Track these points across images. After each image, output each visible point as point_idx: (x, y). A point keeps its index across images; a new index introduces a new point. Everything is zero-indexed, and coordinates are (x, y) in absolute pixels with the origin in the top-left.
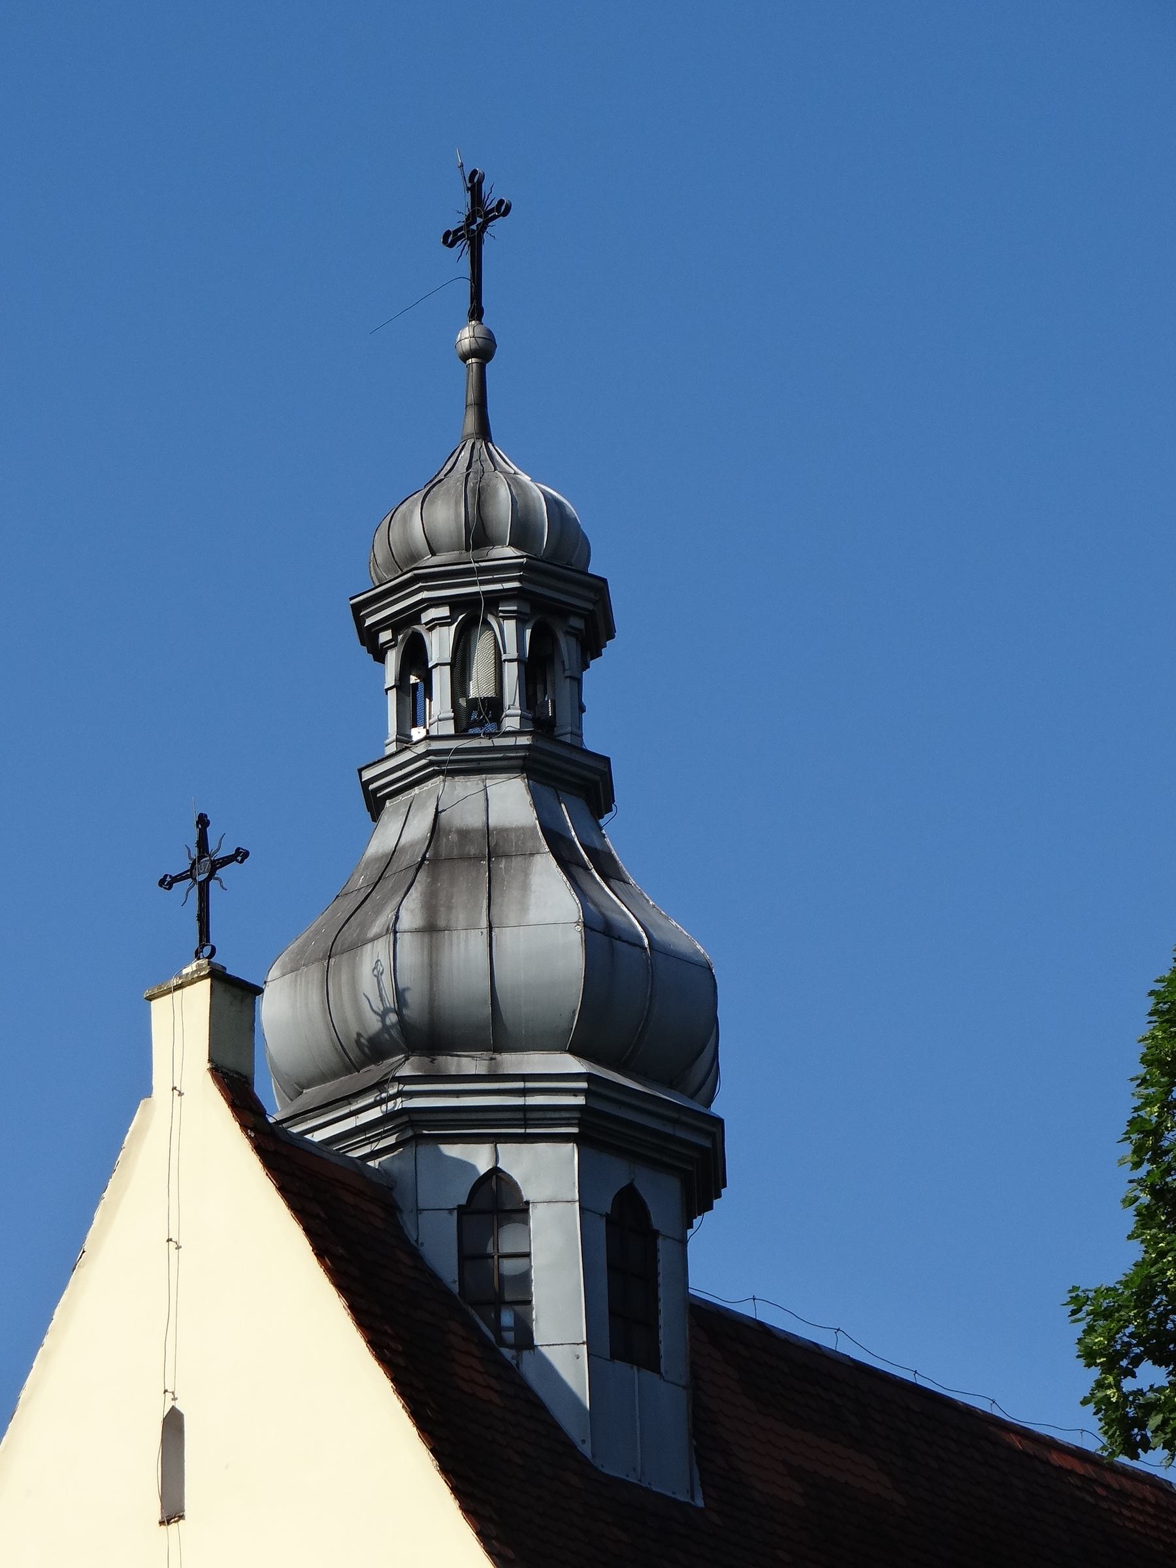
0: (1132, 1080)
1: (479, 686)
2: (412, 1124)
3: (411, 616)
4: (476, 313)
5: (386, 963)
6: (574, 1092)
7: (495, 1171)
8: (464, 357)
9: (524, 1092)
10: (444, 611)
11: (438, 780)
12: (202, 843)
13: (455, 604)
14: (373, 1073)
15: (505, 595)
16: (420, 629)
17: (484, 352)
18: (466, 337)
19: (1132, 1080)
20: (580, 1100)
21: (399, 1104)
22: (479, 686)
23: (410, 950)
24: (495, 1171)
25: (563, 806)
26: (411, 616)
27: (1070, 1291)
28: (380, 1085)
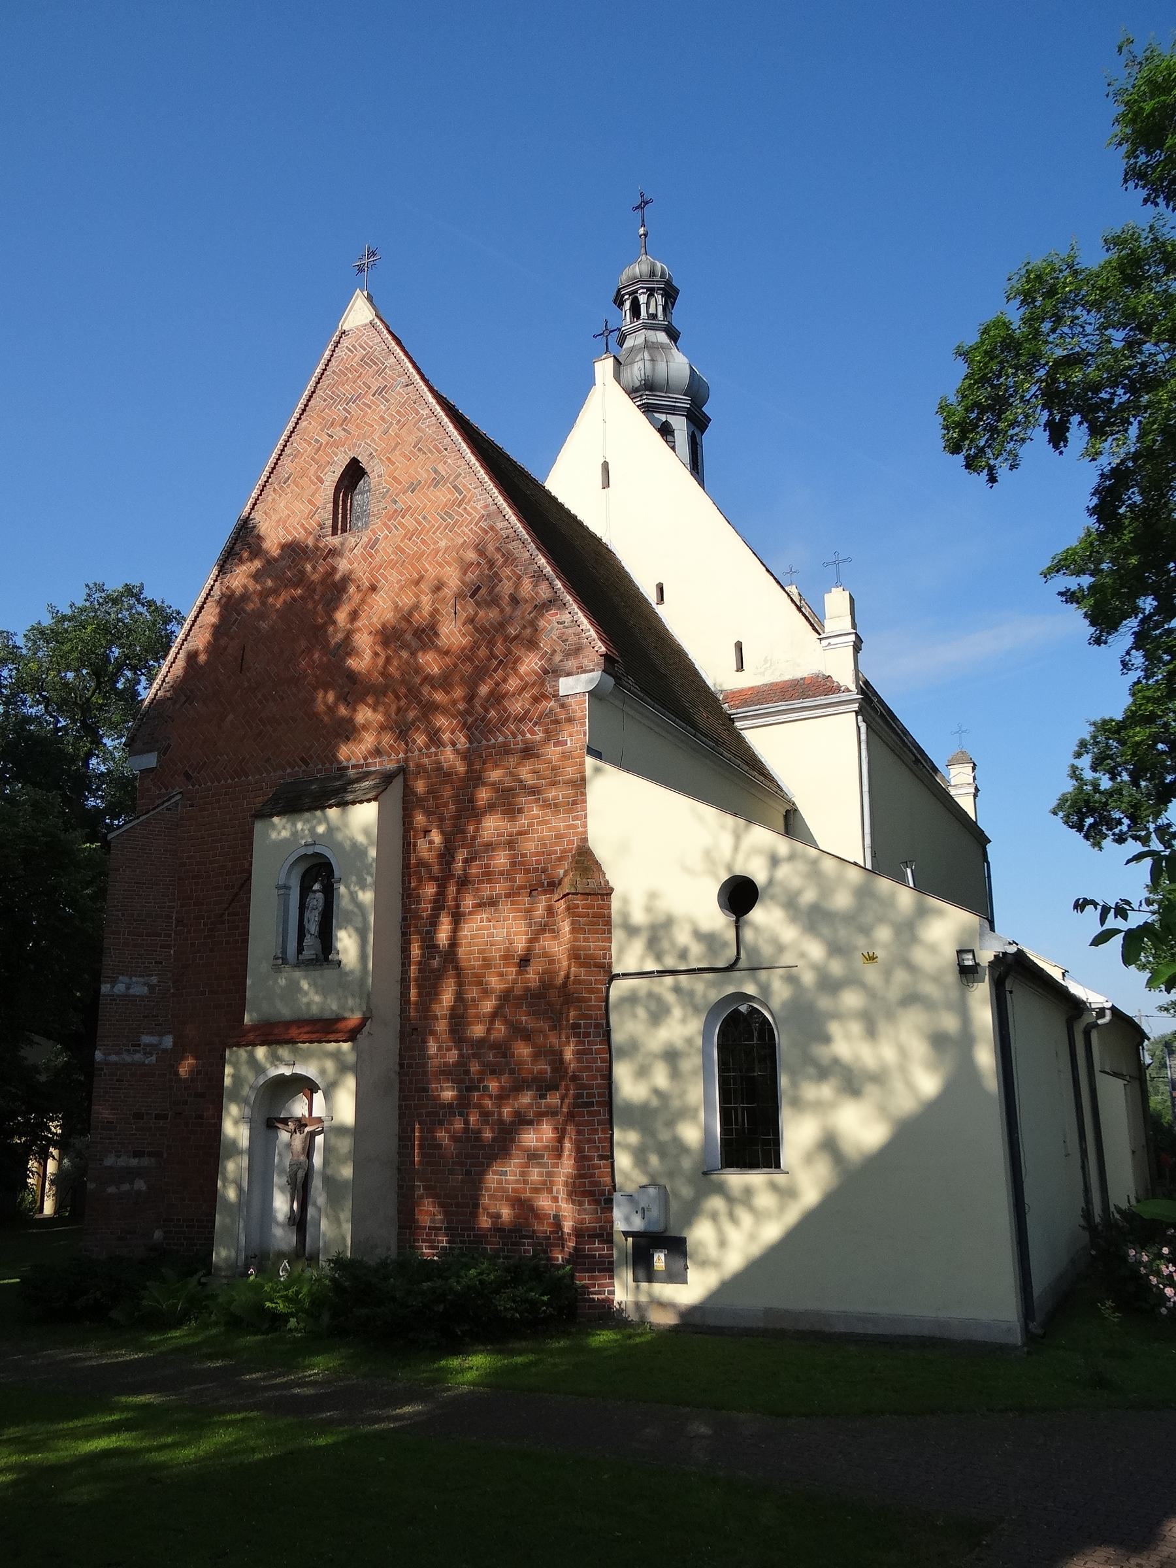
0: (1113, 125)
1: (652, 310)
2: (647, 407)
3: (636, 292)
4: (643, 225)
5: (642, 367)
6: (687, 404)
7: (666, 421)
8: (640, 236)
9: (675, 402)
10: (645, 290)
11: (643, 330)
12: (607, 340)
13: (648, 289)
14: (639, 394)
15: (659, 289)
16: (638, 295)
17: (646, 235)
18: (641, 231)
19: (1113, 125)
20: (688, 406)
21: (646, 401)
22: (652, 310)
23: (648, 364)
24: (666, 421)
25: (18, 1280)
26: (636, 292)
27: (943, 438)
28: (641, 396)
